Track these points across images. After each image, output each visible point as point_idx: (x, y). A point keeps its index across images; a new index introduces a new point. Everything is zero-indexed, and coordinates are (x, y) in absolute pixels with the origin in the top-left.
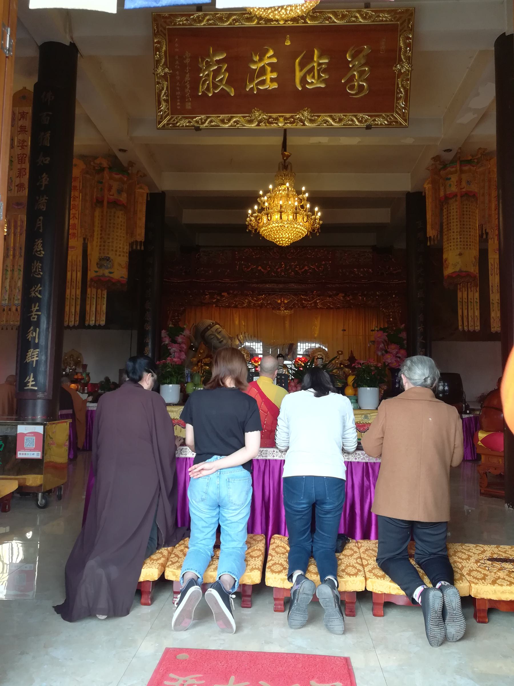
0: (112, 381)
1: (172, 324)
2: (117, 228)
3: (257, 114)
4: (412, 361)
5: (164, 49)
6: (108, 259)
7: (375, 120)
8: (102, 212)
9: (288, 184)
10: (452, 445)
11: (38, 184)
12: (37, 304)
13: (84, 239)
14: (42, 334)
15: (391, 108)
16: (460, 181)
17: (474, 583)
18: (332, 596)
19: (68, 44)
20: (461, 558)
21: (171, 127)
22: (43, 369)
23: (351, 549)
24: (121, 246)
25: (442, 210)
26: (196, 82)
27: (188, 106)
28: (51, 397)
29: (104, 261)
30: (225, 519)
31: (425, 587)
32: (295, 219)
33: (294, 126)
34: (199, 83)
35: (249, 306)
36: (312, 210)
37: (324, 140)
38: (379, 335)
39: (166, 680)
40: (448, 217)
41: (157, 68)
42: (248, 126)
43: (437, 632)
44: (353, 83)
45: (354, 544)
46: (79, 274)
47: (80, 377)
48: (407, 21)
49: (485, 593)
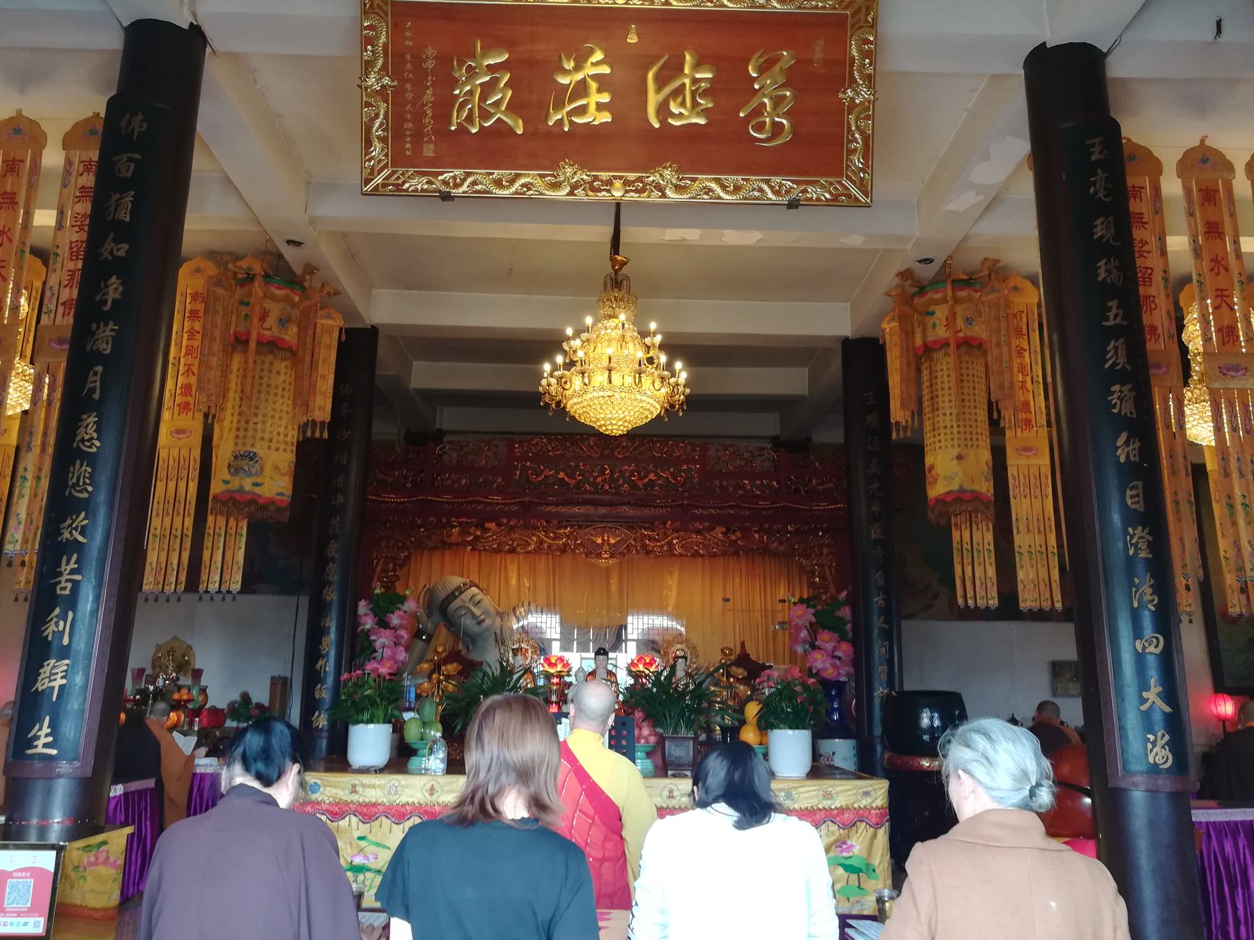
0: (254, 701)
3: (569, 171)
5: (383, 39)
6: (252, 457)
7: (805, 191)
8: (246, 362)
11: (98, 298)
12: (75, 557)
13: (206, 416)
14: (82, 627)
15: (835, 167)
16: (952, 317)
19: (186, 27)
22: (76, 707)
24: (281, 430)
25: (919, 371)
26: (445, 105)
27: (429, 151)
29: (244, 460)
33: (643, 198)
35: (539, 550)
36: (669, 366)
38: (799, 613)
42: (551, 194)
44: (761, 119)
46: (193, 486)
47: (185, 697)
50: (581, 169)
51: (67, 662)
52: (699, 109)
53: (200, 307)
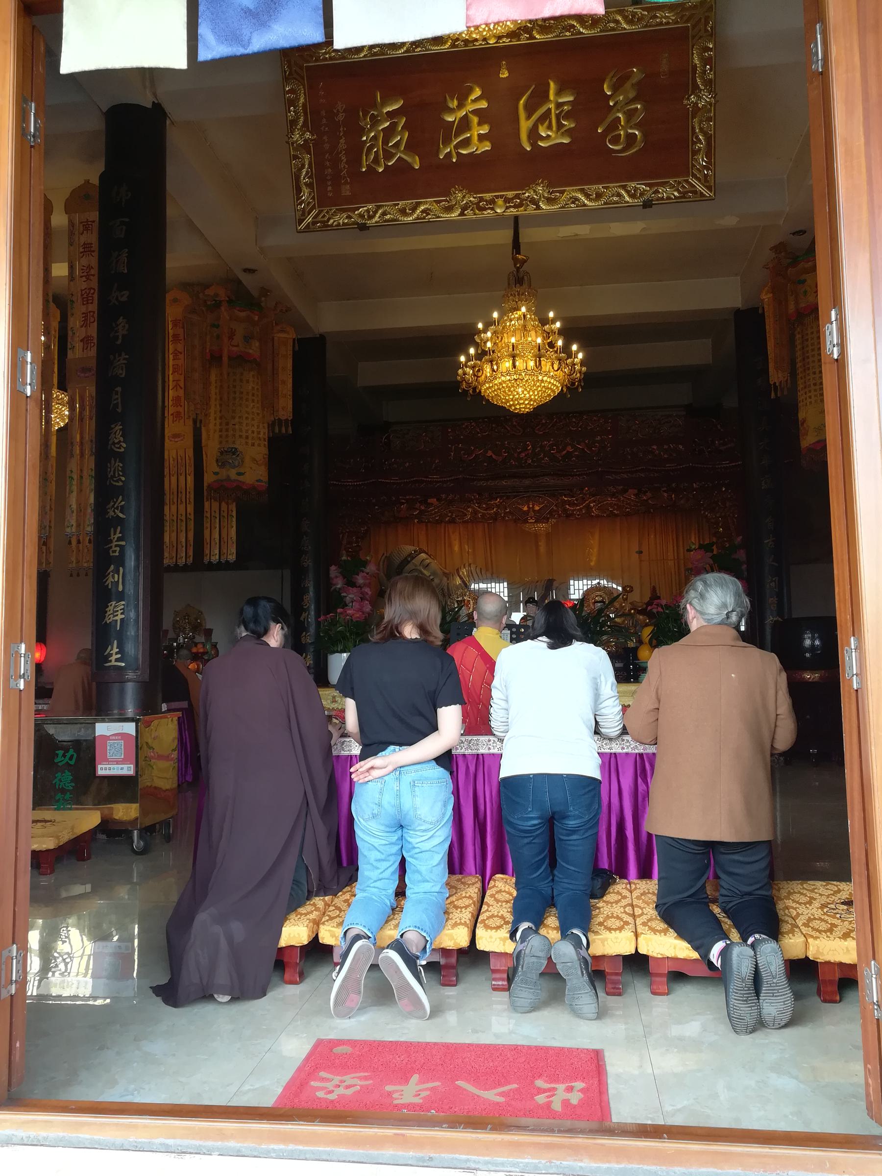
1: (348, 556)
2: (247, 400)
4: (705, 583)
5: (302, 100)
6: (234, 452)
7: (657, 192)
9: (524, 309)
10: (773, 716)
13: (195, 422)
14: (129, 577)
17: (812, 936)
18: (576, 958)
19: (149, 106)
20: (798, 902)
21: (319, 227)
22: (133, 633)
23: (618, 893)
24: (255, 429)
26: (356, 151)
27: (346, 191)
28: (146, 677)
29: (228, 455)
30: (410, 846)
31: (728, 942)
32: (539, 365)
34: (362, 153)
36: (566, 349)
37: (583, 230)
39: (315, 1080)
40: (803, 348)
41: (292, 132)
42: (446, 216)
43: (745, 1011)
45: (624, 886)
46: (190, 479)
47: (201, 650)
48: (703, 20)
49: (831, 952)
50: (469, 192)
51: (123, 603)
52: (563, 130)
53: (180, 331)
